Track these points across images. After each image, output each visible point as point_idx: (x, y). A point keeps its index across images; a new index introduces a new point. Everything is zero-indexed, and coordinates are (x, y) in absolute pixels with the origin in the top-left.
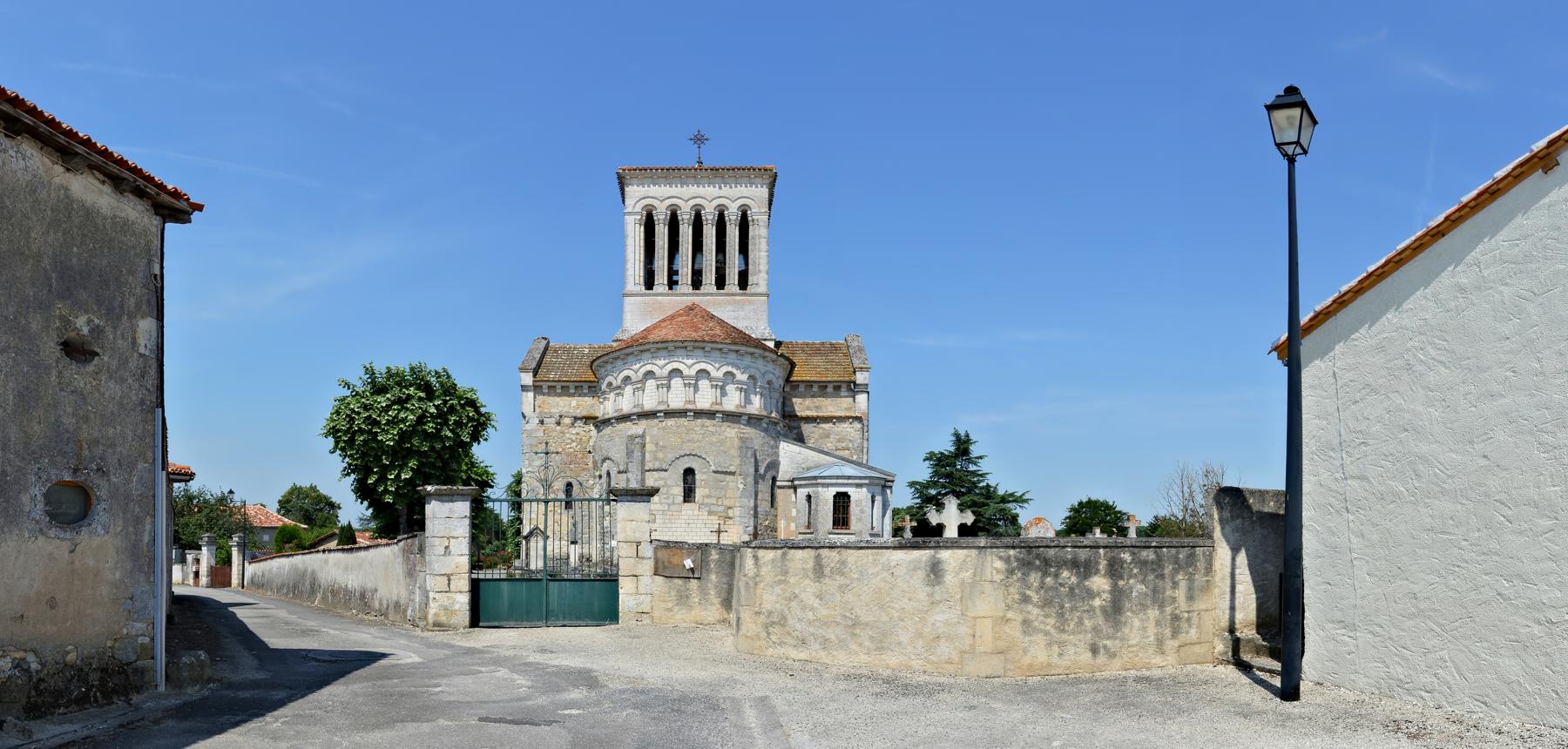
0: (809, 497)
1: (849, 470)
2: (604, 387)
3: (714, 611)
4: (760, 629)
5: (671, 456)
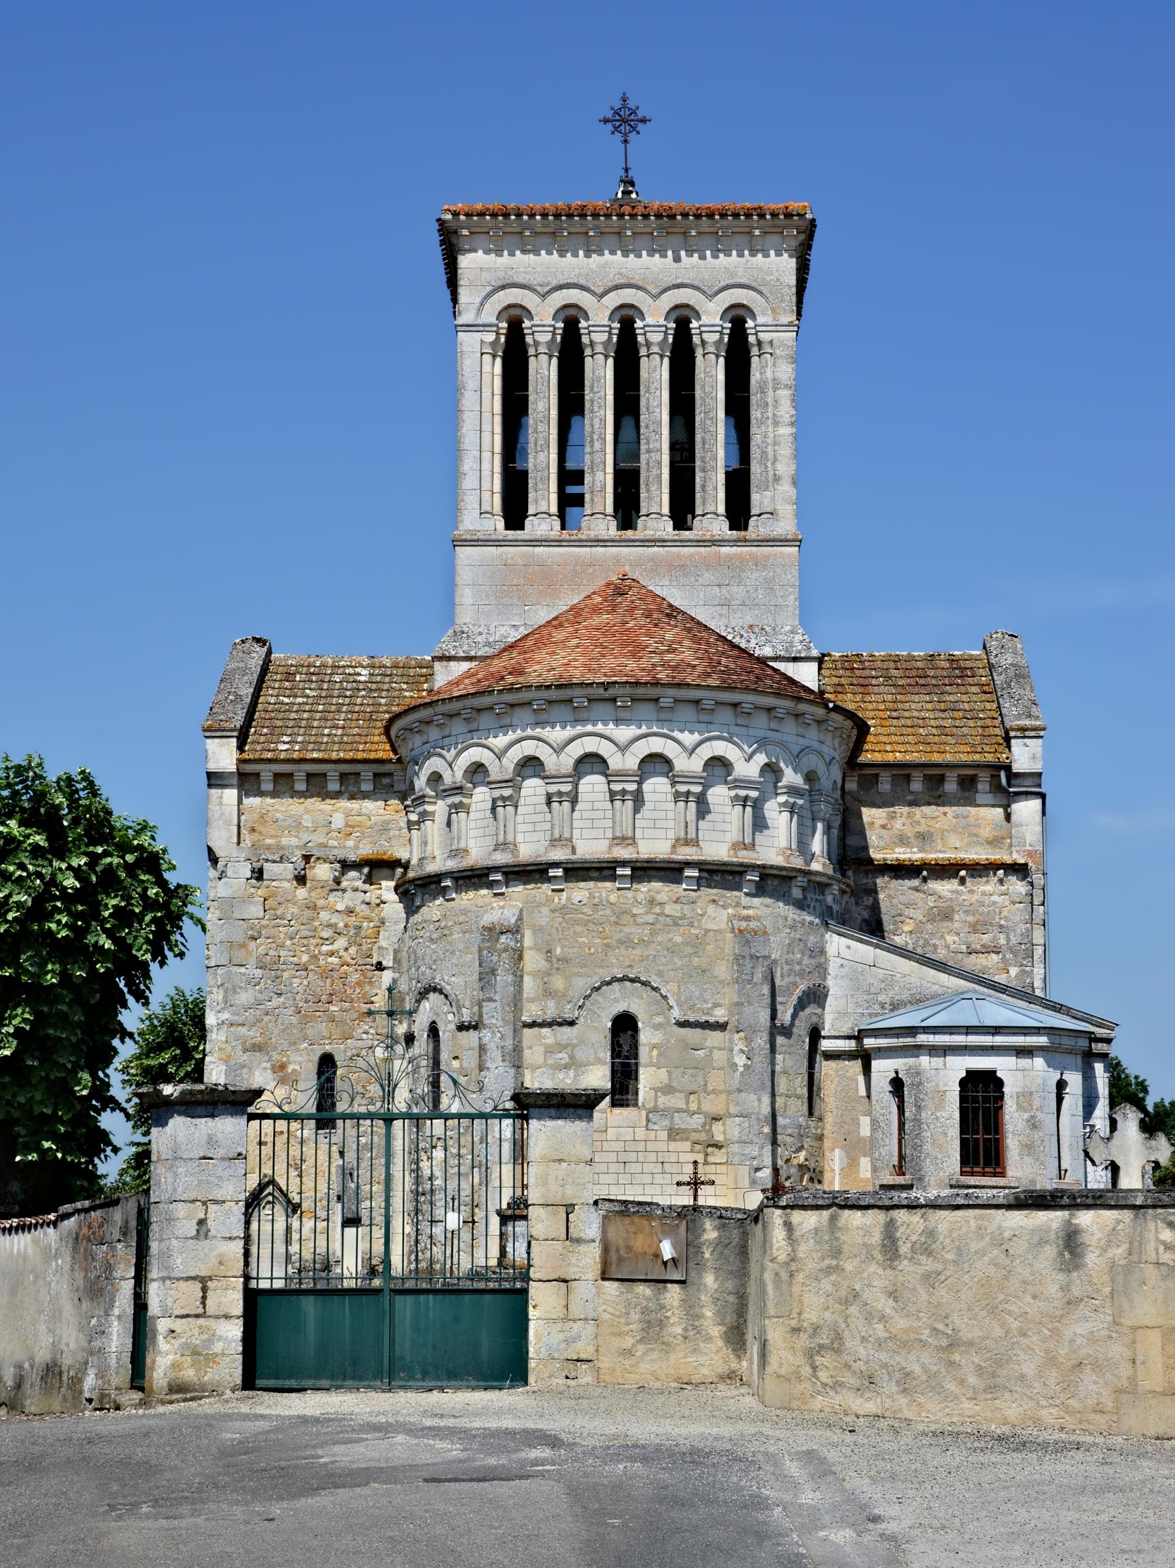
0: (897, 1085)
1: (998, 1012)
2: (420, 783)
3: (714, 1355)
4: (800, 1360)
5: (582, 984)
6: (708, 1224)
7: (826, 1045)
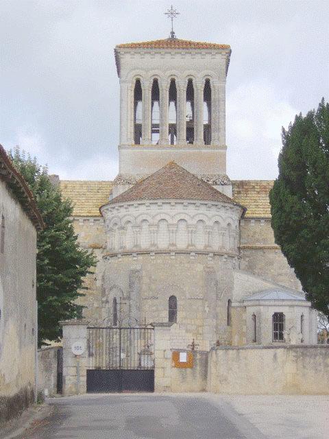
6: (198, 355)
7: (233, 304)
